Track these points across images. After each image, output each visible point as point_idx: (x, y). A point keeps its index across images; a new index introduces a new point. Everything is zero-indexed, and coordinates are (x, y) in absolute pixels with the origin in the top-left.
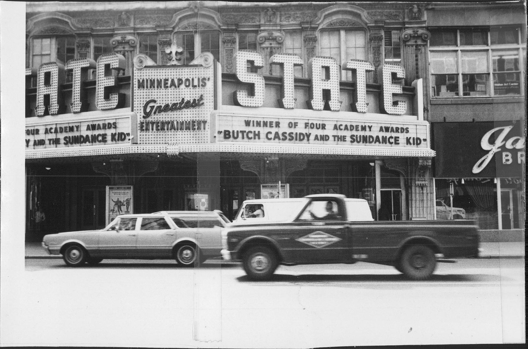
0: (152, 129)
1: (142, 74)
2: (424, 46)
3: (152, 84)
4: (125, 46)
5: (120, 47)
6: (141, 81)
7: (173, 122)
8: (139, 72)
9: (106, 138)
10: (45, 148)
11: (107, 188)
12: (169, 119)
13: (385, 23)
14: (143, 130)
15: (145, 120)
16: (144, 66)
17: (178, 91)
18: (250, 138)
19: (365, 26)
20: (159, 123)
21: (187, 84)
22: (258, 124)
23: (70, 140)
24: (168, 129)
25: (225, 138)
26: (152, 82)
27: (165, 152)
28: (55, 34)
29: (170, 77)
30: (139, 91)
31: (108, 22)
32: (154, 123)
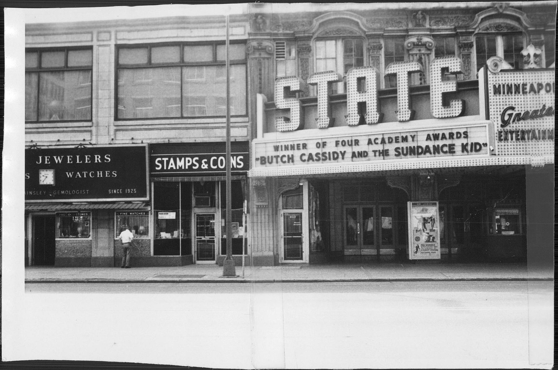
0: (512, 139)
1: (497, 79)
2: (268, 59)
3: (510, 89)
4: (422, 49)
5: (416, 49)
6: (497, 86)
7: (534, 131)
8: (494, 76)
9: (454, 148)
10: (369, 160)
11: (409, 204)
12: (530, 128)
13: (385, 31)
14: (502, 140)
15: (502, 129)
16: (499, 70)
17: (537, 96)
18: (285, 162)
19: (363, 35)
20: (518, 132)
21: (548, 89)
22: (293, 147)
23: (403, 151)
24: (528, 139)
25: (262, 163)
26: (509, 88)
27: (528, 163)
28: (341, 35)
29: (528, 81)
30: (495, 97)
31: (400, 22)
32: (513, 132)
